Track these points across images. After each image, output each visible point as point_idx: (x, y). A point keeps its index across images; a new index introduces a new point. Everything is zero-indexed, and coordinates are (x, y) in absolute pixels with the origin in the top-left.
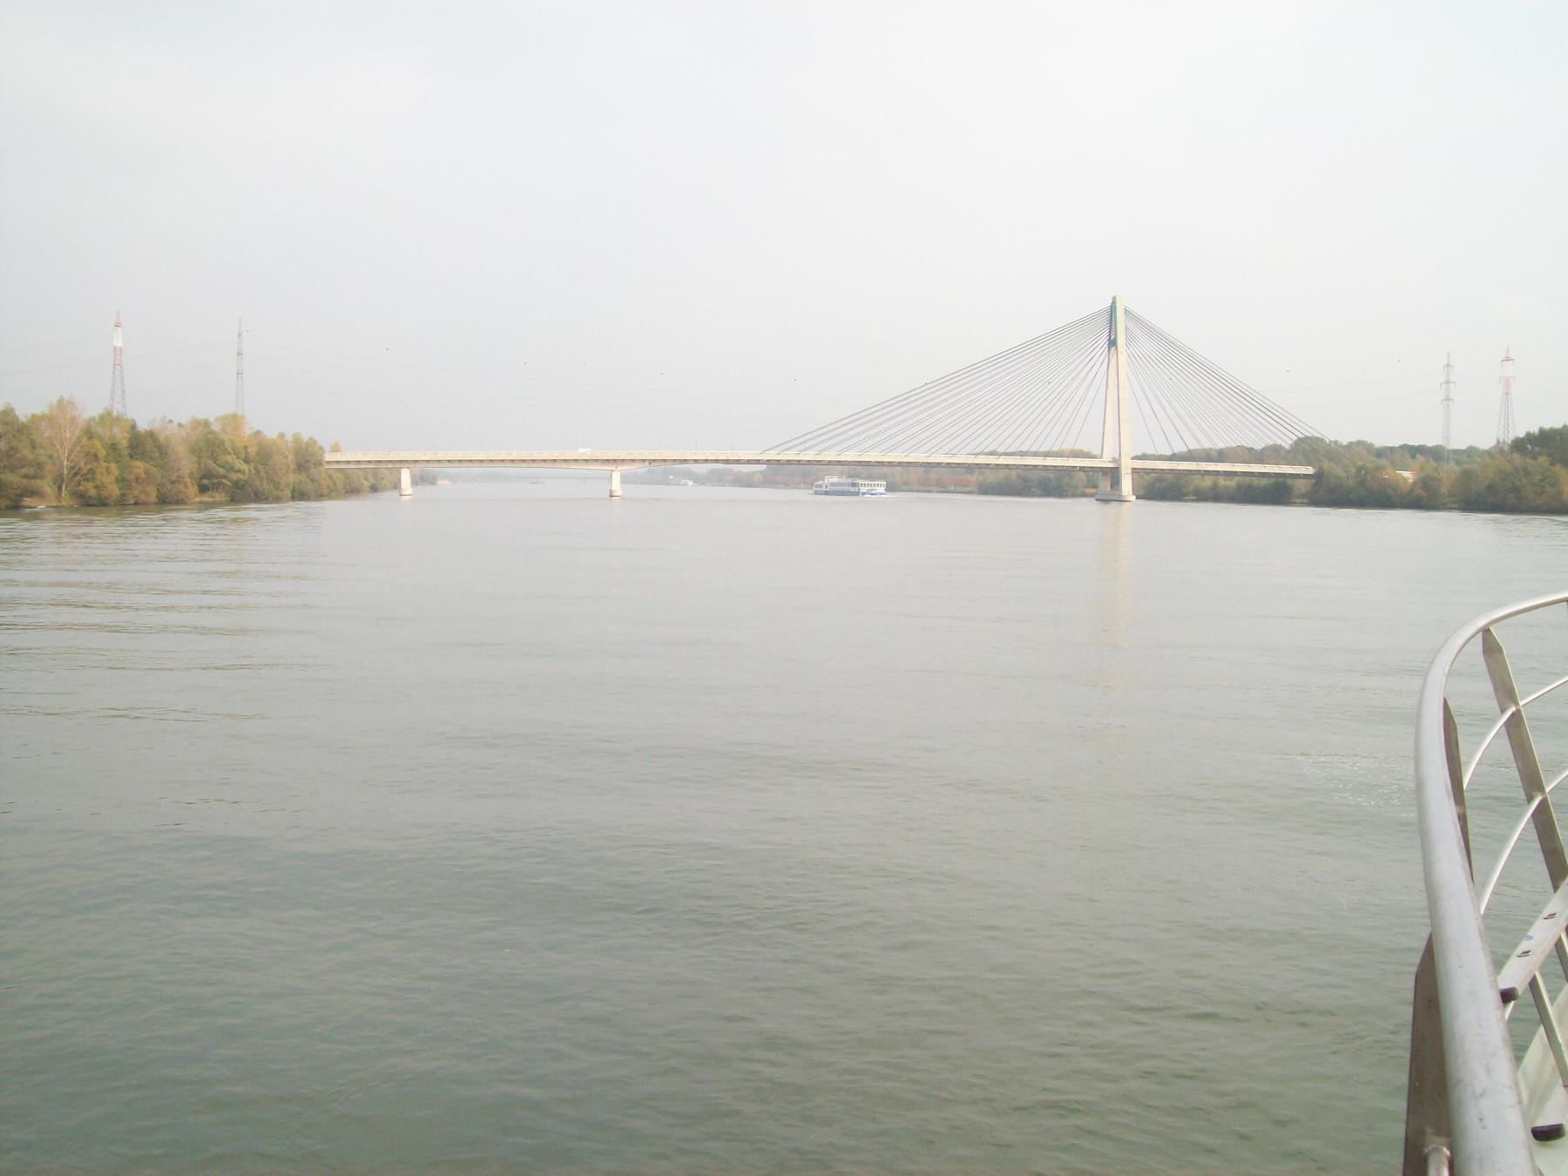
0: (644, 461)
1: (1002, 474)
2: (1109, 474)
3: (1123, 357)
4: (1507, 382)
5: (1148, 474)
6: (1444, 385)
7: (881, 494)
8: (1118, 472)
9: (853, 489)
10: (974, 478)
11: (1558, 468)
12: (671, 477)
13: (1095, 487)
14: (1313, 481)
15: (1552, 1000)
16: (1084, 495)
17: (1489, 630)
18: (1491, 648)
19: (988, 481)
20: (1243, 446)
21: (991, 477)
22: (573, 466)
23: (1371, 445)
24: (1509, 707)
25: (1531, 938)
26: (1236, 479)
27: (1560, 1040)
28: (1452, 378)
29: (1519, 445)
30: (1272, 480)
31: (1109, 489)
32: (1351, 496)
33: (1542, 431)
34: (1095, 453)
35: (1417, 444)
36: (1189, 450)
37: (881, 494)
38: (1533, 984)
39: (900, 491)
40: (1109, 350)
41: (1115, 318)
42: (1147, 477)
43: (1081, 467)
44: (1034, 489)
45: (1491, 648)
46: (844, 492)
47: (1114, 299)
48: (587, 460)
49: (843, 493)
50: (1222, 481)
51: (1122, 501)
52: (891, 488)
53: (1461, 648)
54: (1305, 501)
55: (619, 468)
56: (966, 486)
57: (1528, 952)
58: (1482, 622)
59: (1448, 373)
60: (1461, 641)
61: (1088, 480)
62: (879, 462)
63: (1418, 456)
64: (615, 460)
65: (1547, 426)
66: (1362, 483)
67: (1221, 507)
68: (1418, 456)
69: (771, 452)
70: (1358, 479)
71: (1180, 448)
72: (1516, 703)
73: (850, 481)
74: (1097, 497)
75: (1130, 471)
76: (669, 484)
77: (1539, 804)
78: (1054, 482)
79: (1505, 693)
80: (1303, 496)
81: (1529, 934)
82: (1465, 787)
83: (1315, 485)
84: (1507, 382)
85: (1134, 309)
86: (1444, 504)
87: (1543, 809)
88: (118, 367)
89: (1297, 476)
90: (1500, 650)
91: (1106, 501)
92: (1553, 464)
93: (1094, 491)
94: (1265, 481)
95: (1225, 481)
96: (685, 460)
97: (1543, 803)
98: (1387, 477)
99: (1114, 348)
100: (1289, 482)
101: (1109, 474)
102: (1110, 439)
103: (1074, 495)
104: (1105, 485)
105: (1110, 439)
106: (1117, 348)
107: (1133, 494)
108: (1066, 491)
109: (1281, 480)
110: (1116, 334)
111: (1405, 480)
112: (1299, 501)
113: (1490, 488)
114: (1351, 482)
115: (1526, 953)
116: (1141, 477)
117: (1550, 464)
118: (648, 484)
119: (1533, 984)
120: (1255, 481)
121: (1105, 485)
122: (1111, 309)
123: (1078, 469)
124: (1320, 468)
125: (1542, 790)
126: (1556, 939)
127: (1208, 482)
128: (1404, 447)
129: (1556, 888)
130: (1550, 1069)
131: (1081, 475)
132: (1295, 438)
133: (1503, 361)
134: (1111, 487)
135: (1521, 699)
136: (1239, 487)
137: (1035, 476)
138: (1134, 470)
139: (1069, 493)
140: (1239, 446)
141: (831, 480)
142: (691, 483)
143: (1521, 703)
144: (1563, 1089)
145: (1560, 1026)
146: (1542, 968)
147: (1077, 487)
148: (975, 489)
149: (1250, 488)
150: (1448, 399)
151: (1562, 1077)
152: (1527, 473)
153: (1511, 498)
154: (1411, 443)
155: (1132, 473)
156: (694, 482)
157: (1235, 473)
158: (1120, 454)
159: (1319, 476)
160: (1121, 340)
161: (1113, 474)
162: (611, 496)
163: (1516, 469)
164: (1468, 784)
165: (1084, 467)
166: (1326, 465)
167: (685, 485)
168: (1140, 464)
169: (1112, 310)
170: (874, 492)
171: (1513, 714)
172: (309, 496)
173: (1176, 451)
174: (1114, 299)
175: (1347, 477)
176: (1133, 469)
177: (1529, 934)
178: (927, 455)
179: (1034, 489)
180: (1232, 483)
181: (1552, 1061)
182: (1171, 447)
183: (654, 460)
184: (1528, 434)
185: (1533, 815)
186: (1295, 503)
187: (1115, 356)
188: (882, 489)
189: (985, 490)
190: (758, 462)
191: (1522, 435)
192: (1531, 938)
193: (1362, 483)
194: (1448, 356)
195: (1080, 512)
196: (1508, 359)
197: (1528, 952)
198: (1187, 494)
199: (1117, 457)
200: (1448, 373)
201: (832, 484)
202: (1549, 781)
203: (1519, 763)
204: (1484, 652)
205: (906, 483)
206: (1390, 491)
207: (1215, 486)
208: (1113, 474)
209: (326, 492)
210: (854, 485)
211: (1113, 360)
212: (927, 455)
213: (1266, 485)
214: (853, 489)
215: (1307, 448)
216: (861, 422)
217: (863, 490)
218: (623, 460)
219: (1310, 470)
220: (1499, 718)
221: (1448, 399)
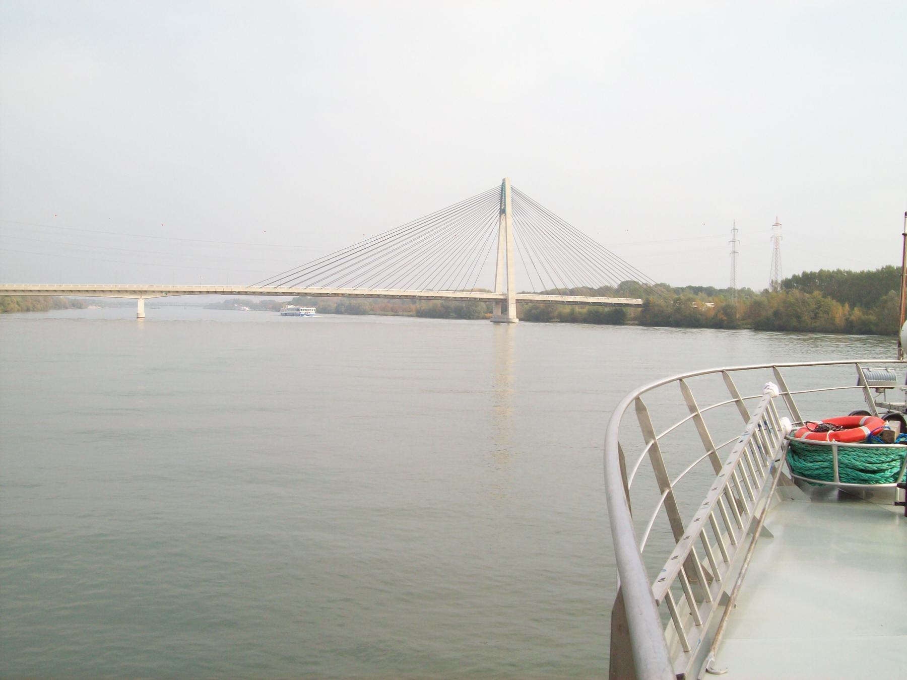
0: (162, 292)
1: (431, 304)
2: (501, 303)
3: (510, 221)
4: (776, 241)
5: (527, 303)
6: (731, 243)
7: (313, 315)
8: (507, 302)
9: (298, 312)
11: (829, 299)
12: (236, 305)
13: (491, 312)
14: (640, 309)
15: (677, 604)
16: (485, 318)
17: (639, 398)
18: (639, 407)
19: (423, 308)
20: (587, 287)
21: (424, 305)
22: (109, 295)
23: (669, 286)
24: (650, 441)
25: (665, 570)
26: (587, 307)
27: (682, 627)
28: (737, 238)
29: (788, 284)
30: (612, 309)
31: (500, 313)
32: (671, 319)
33: (804, 274)
34: (492, 291)
35: (697, 286)
36: (557, 289)
37: (313, 315)
38: (667, 597)
39: (369, 315)
40: (500, 216)
41: (505, 194)
42: (526, 306)
43: (480, 299)
44: (452, 314)
45: (639, 407)
46: (293, 314)
47: (504, 180)
48: (119, 291)
49: (293, 315)
50: (577, 309)
51: (509, 322)
52: (318, 312)
53: (625, 410)
54: (636, 322)
55: (143, 297)
56: (409, 311)
57: (664, 579)
58: (635, 394)
59: (734, 235)
60: (625, 405)
61: (488, 308)
62: (335, 294)
63: (700, 293)
64: (140, 291)
65: (808, 271)
66: (678, 310)
67: (575, 325)
68: (700, 293)
69: (255, 286)
70: (675, 308)
71: (550, 287)
72: (654, 438)
73: (295, 307)
74: (492, 319)
76: (234, 309)
77: (667, 494)
79: (649, 434)
80: (634, 319)
81: (664, 568)
82: (629, 488)
83: (643, 312)
84: (776, 241)
85: (519, 188)
86: (739, 325)
87: (670, 497)
88: (481, 300)
89: (630, 305)
90: (645, 409)
91: (497, 322)
92: (825, 296)
93: (491, 315)
94: (607, 309)
95: (579, 308)
96: (192, 292)
97: (670, 494)
98: (696, 306)
99: (504, 214)
100: (624, 309)
101: (501, 303)
102: (501, 278)
103: (478, 318)
104: (497, 311)
105: (501, 278)
106: (505, 215)
107: (517, 318)
108: (472, 315)
109: (618, 308)
110: (505, 205)
111: (709, 309)
112: (631, 323)
113: (776, 314)
114: (670, 310)
115: (663, 579)
116: (522, 306)
117: (823, 297)
118: (224, 309)
119: (667, 597)
120: (600, 309)
121: (497, 311)
122: (502, 189)
123: (478, 299)
124: (647, 300)
125: (668, 486)
126: (678, 571)
127: (567, 310)
128: (690, 287)
129: (677, 541)
130: (676, 642)
131: (482, 304)
132: (619, 282)
133: (773, 226)
134: (502, 313)
135: (657, 435)
136: (590, 312)
137: (454, 304)
138: (517, 301)
140: (583, 287)
141: (289, 307)
142: (247, 309)
143: (657, 438)
144: (684, 653)
145: (681, 617)
146: (672, 588)
148: (414, 313)
150: (734, 252)
151: (683, 647)
152: (804, 301)
153: (794, 322)
154: (693, 285)
155: (516, 302)
156: (249, 308)
157: (588, 303)
158: (508, 290)
159: (646, 306)
160: (509, 209)
161: (503, 303)
162: (138, 318)
163: (797, 300)
164: (631, 485)
165: (482, 299)
166: (651, 298)
167: (244, 310)
168: (522, 297)
170: (309, 314)
171: (653, 445)
172: (675, 292)
173: (547, 289)
174: (504, 180)
175: (667, 306)
177: (664, 568)
178: (353, 288)
180: (585, 310)
181: (677, 637)
182: (544, 287)
183: (169, 292)
184: (794, 276)
185: (664, 501)
186: (629, 324)
187: (504, 219)
188: (313, 312)
189: (420, 314)
190: (291, 294)
191: (790, 277)
192: (665, 570)
193: (678, 310)
194: (734, 223)
195: (480, 328)
196: (777, 224)
197: (664, 579)
198: (553, 318)
200: (734, 235)
201: (289, 309)
202: (672, 481)
203: (656, 472)
204: (636, 410)
205: (372, 310)
206: (699, 316)
207: (572, 312)
208: (503, 303)
209: (31, 307)
210: (298, 310)
211: (503, 223)
212: (353, 288)
213: (608, 311)
214: (298, 312)
215: (629, 288)
216: (571, 236)
217: (303, 312)
218: (146, 291)
219: (640, 301)
220: (646, 447)
221: (734, 252)
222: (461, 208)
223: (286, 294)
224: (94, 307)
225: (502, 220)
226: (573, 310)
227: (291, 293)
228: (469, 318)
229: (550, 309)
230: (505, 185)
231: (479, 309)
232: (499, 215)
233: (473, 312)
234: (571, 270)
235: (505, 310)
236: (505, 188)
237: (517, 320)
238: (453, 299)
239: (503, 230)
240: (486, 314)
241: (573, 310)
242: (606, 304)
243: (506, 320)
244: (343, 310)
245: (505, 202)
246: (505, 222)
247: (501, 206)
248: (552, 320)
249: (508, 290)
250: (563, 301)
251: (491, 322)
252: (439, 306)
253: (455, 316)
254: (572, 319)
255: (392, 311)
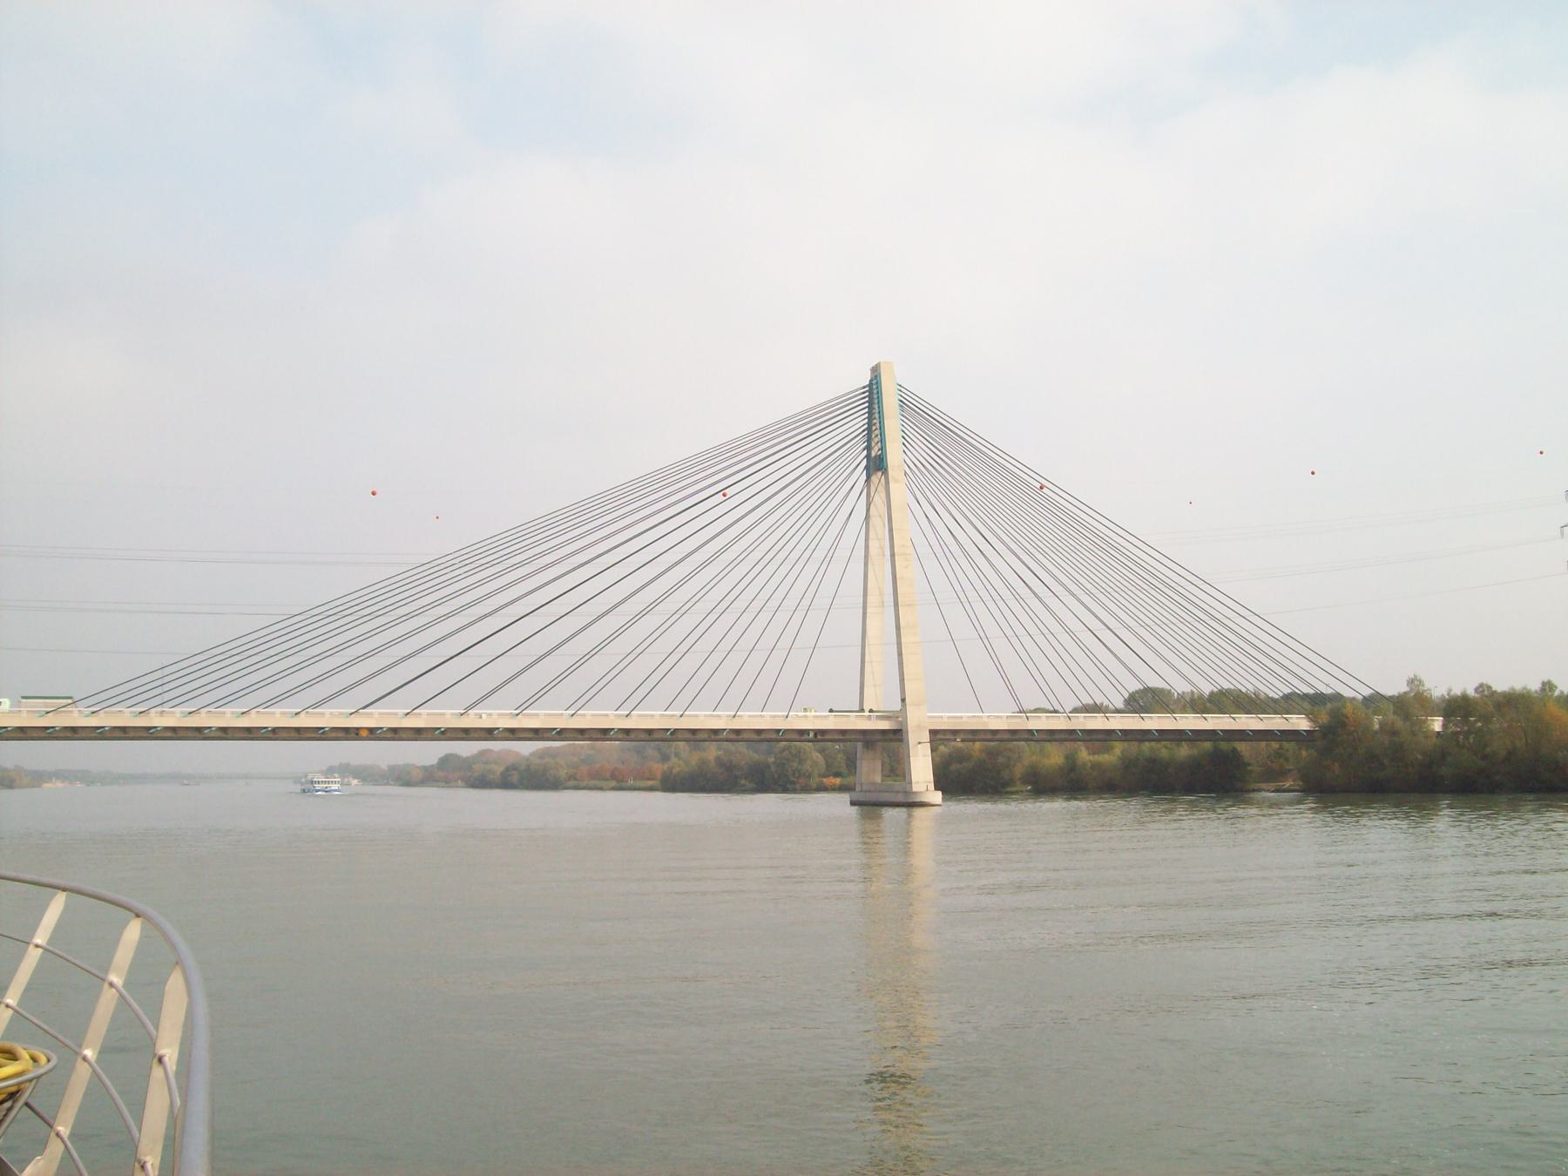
1: (712, 752)
3: (899, 489)
10: (131, 734)
16: (822, 789)
31: (878, 778)
47: (876, 370)
56: (649, 779)
61: (828, 766)
69: (277, 710)
75: (926, 737)
78: (773, 768)
88: (819, 737)
94: (1184, 751)
100: (1242, 747)
103: (806, 789)
104: (870, 771)
108: (793, 783)
110: (882, 441)
120: (1163, 751)
122: (870, 391)
123: (812, 735)
136: (1128, 764)
139: (798, 786)
142: (355, 782)
147: (809, 776)
149: (1153, 764)
158: (903, 700)
160: (895, 455)
161: (890, 742)
169: (873, 393)
170: (329, 789)
176: (933, 733)
179: (743, 782)
180: (1112, 757)
187: (881, 488)
199: (897, 706)
207: (1071, 766)
208: (890, 742)
211: (879, 499)
222: (996, 511)
223: (181, 734)
224: (59, 785)
225: (873, 489)
226: (1071, 758)
227: (249, 730)
228: (785, 790)
229: (1001, 760)
230: (879, 384)
231: (807, 766)
232: (864, 477)
233: (794, 774)
234: (1009, 633)
235: (897, 768)
236: (879, 393)
237: (937, 797)
238: (733, 736)
239: (879, 524)
240: (825, 780)
241: (1071, 758)
242: (1178, 736)
243: (900, 798)
244: (515, 778)
245: (882, 434)
246: (883, 495)
247: (869, 448)
248: (1009, 789)
249: (903, 700)
250: (1073, 732)
251: (853, 803)
252: (713, 764)
253: (752, 785)
254: (1043, 785)
255: (613, 777)
